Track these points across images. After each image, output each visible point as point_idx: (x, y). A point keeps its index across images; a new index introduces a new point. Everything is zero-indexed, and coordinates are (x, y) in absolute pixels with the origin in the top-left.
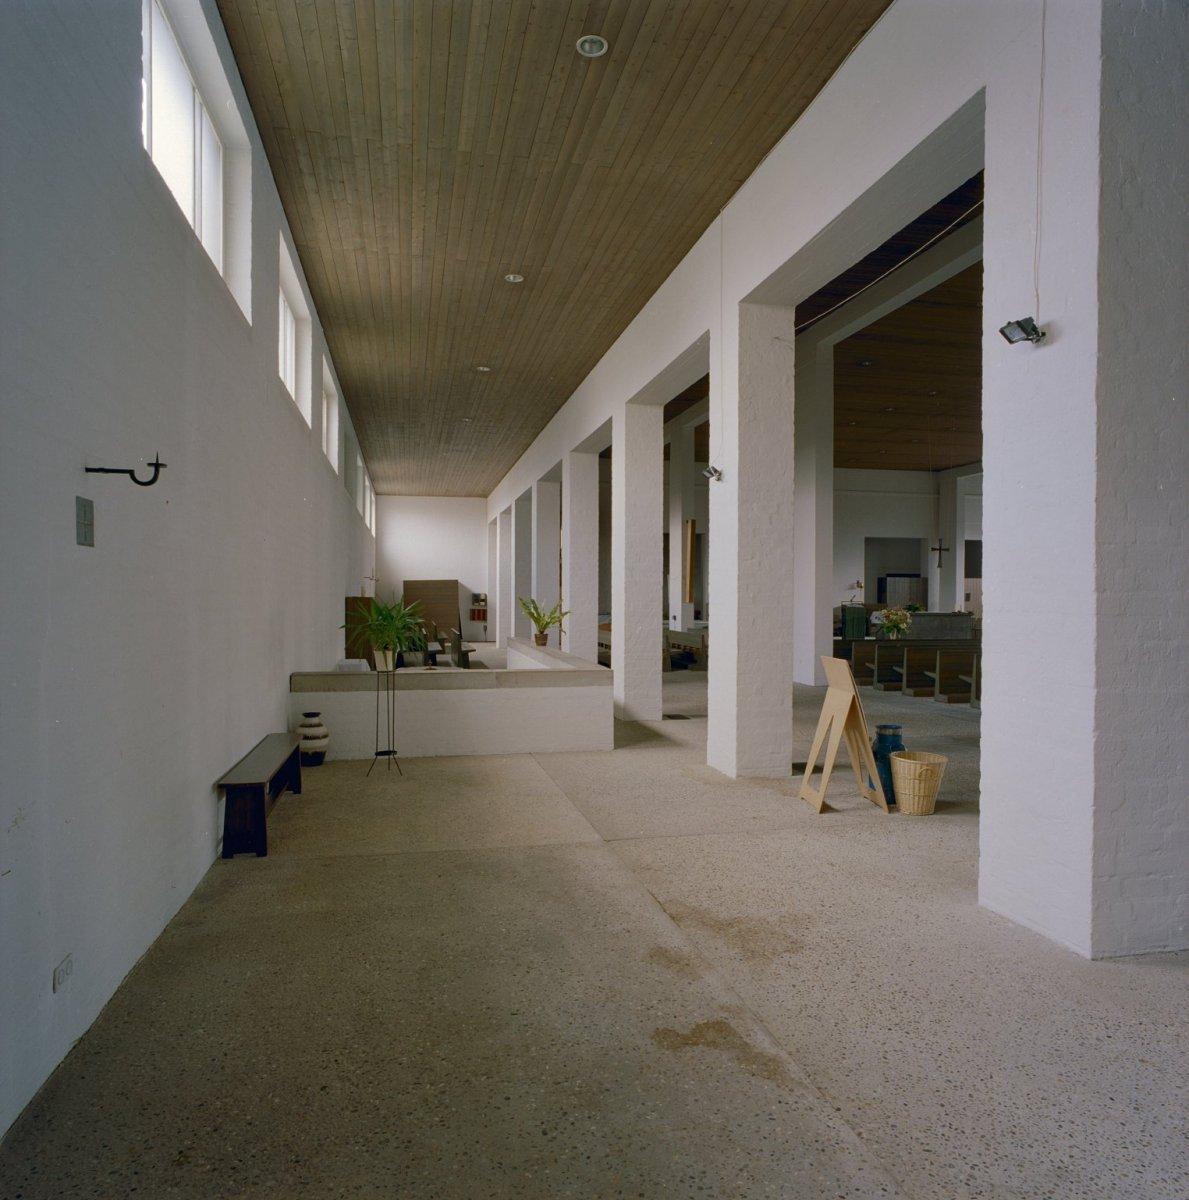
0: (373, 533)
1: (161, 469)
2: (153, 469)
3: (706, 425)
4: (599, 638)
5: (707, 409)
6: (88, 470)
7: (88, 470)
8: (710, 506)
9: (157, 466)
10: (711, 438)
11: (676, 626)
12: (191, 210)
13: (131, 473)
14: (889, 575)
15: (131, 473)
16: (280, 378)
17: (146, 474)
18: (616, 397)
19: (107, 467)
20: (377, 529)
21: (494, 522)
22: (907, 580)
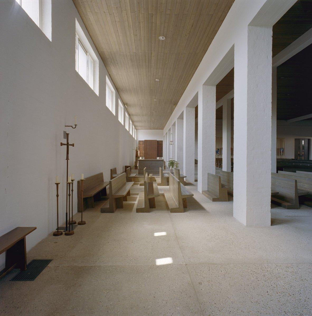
0: (136, 139)
1: (77, 126)
2: (75, 126)
3: (232, 100)
4: (273, 185)
5: (233, 93)
6: (65, 126)
7: (65, 126)
8: (271, 72)
9: (76, 125)
10: (234, 105)
11: (217, 158)
12: (111, 109)
13: (72, 126)
14: (67, 181)
15: (72, 126)
16: (119, 121)
17: (74, 127)
18: (186, 99)
19: (68, 126)
20: (137, 138)
21: (164, 136)
22: (131, 170)
